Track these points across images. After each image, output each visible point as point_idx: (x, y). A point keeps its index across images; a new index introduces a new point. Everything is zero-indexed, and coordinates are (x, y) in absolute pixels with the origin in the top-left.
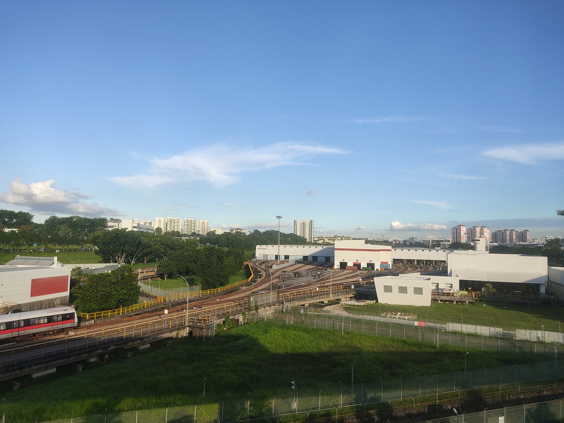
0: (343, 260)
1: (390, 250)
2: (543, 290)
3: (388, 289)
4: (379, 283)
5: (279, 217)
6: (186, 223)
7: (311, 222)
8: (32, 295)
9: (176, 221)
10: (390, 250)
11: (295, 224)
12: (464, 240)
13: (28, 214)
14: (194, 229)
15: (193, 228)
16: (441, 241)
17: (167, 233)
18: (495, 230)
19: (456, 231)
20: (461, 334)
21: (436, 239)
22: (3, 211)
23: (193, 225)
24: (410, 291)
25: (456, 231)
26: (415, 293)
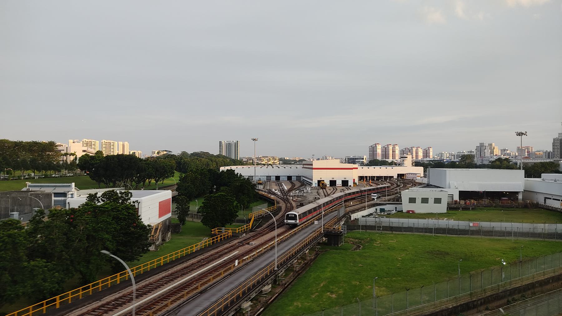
0: (333, 178)
1: (357, 168)
2: (520, 197)
4: (406, 194)
6: (104, 146)
7: (236, 144)
8: (160, 216)
9: (93, 143)
10: (357, 168)
11: (220, 146)
12: (379, 158)
13: (51, 146)
14: (113, 152)
15: (112, 150)
16: (356, 159)
17: (108, 157)
18: (403, 148)
20: (214, 249)
21: (351, 157)
22: (2, 140)
23: (112, 147)
24: (431, 201)
25: (373, 150)
26: (435, 203)
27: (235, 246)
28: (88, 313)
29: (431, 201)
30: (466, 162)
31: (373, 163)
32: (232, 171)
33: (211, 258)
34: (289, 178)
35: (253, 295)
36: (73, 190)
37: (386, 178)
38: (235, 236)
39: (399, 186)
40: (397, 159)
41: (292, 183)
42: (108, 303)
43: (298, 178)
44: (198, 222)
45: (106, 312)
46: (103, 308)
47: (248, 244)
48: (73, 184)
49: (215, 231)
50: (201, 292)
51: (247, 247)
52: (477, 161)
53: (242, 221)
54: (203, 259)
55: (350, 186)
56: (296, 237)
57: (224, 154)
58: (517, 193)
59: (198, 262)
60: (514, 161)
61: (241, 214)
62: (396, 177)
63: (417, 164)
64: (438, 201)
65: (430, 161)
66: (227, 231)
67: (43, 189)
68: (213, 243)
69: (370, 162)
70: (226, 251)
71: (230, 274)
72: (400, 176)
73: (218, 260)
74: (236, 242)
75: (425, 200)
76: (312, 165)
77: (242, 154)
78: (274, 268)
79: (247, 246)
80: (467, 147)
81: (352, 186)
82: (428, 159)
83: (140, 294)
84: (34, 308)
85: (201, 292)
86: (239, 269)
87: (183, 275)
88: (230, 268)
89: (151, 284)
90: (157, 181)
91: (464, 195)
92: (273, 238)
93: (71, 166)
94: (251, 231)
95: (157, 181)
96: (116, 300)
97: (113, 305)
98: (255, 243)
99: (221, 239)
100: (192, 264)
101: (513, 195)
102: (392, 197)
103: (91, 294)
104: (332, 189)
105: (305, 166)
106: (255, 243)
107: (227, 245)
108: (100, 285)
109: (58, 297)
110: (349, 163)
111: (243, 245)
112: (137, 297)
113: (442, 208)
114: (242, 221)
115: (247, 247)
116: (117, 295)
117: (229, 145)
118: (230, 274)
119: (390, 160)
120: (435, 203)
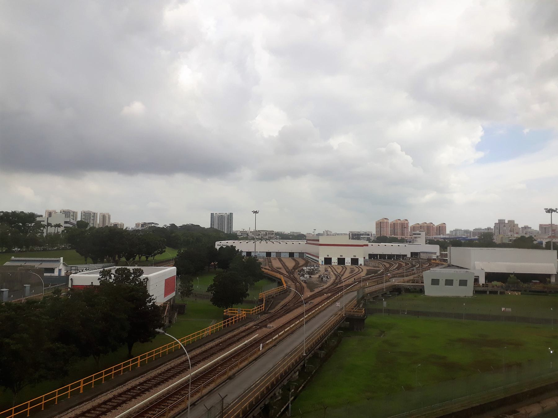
1: (367, 245)
2: (553, 280)
3: (435, 282)
5: (256, 212)
8: (166, 295)
10: (367, 245)
16: (361, 235)
19: (380, 225)
24: (456, 283)
26: (460, 285)
27: (252, 330)
28: (83, 414)
29: (456, 283)
30: (485, 240)
31: (381, 239)
32: (233, 248)
33: (229, 342)
34: (291, 255)
35: (285, 382)
36: (62, 265)
37: (398, 256)
38: (248, 319)
39: (415, 266)
40: (407, 237)
41: (294, 260)
42: (133, 388)
43: (301, 254)
44: (206, 303)
45: (104, 413)
46: (99, 409)
47: (266, 326)
48: (62, 258)
49: (227, 311)
50: (230, 378)
51: (265, 331)
52: (497, 239)
53: (252, 303)
54: (221, 343)
55: (361, 265)
56: (295, 336)
57: (216, 227)
58: (549, 276)
59: (217, 345)
60: (539, 240)
61: (252, 295)
62: (409, 256)
63: (430, 242)
64: (463, 283)
65: (444, 239)
66: (239, 312)
67: (28, 264)
68: (224, 326)
69: (378, 238)
70: (244, 334)
71: (256, 359)
72: (414, 254)
73: (202, 363)
74: (251, 324)
75: (449, 282)
76: (318, 240)
77: (237, 227)
78: (303, 353)
79: (264, 329)
80: (486, 222)
81: (363, 264)
82: (442, 236)
83: (196, 361)
84: (85, 382)
85: (230, 378)
86: (263, 354)
87: (222, 350)
88: (255, 352)
89: (149, 380)
90: (147, 258)
91: (490, 277)
92: (301, 315)
93: (53, 240)
94: (264, 313)
95: (147, 258)
96: (141, 384)
97: (139, 389)
98: (273, 326)
99: (235, 321)
100: (211, 348)
101: (544, 278)
102: (411, 277)
103: (139, 366)
104: (341, 268)
105: (308, 242)
106: (273, 326)
107: (243, 328)
108: (29, 408)
109: (82, 380)
110: (353, 239)
111: (260, 328)
112: (193, 365)
113: (468, 291)
114: (252, 303)
115: (265, 331)
116: (141, 380)
117: (221, 218)
118: (256, 359)
119: (399, 237)
120: (460, 285)
